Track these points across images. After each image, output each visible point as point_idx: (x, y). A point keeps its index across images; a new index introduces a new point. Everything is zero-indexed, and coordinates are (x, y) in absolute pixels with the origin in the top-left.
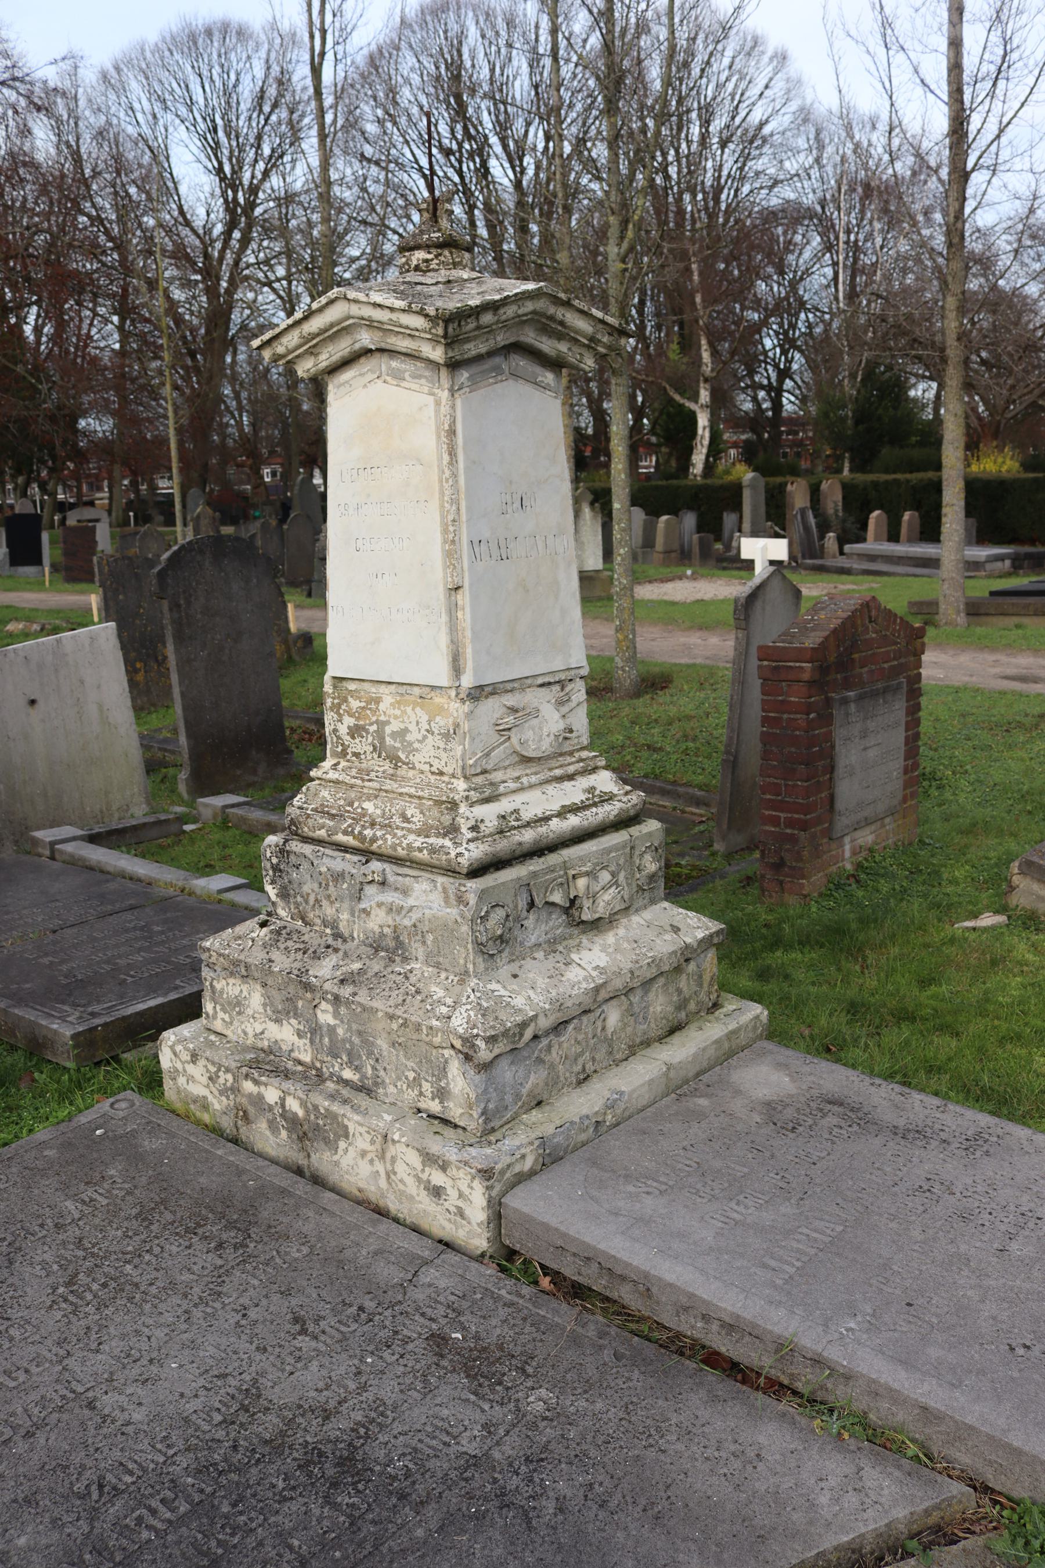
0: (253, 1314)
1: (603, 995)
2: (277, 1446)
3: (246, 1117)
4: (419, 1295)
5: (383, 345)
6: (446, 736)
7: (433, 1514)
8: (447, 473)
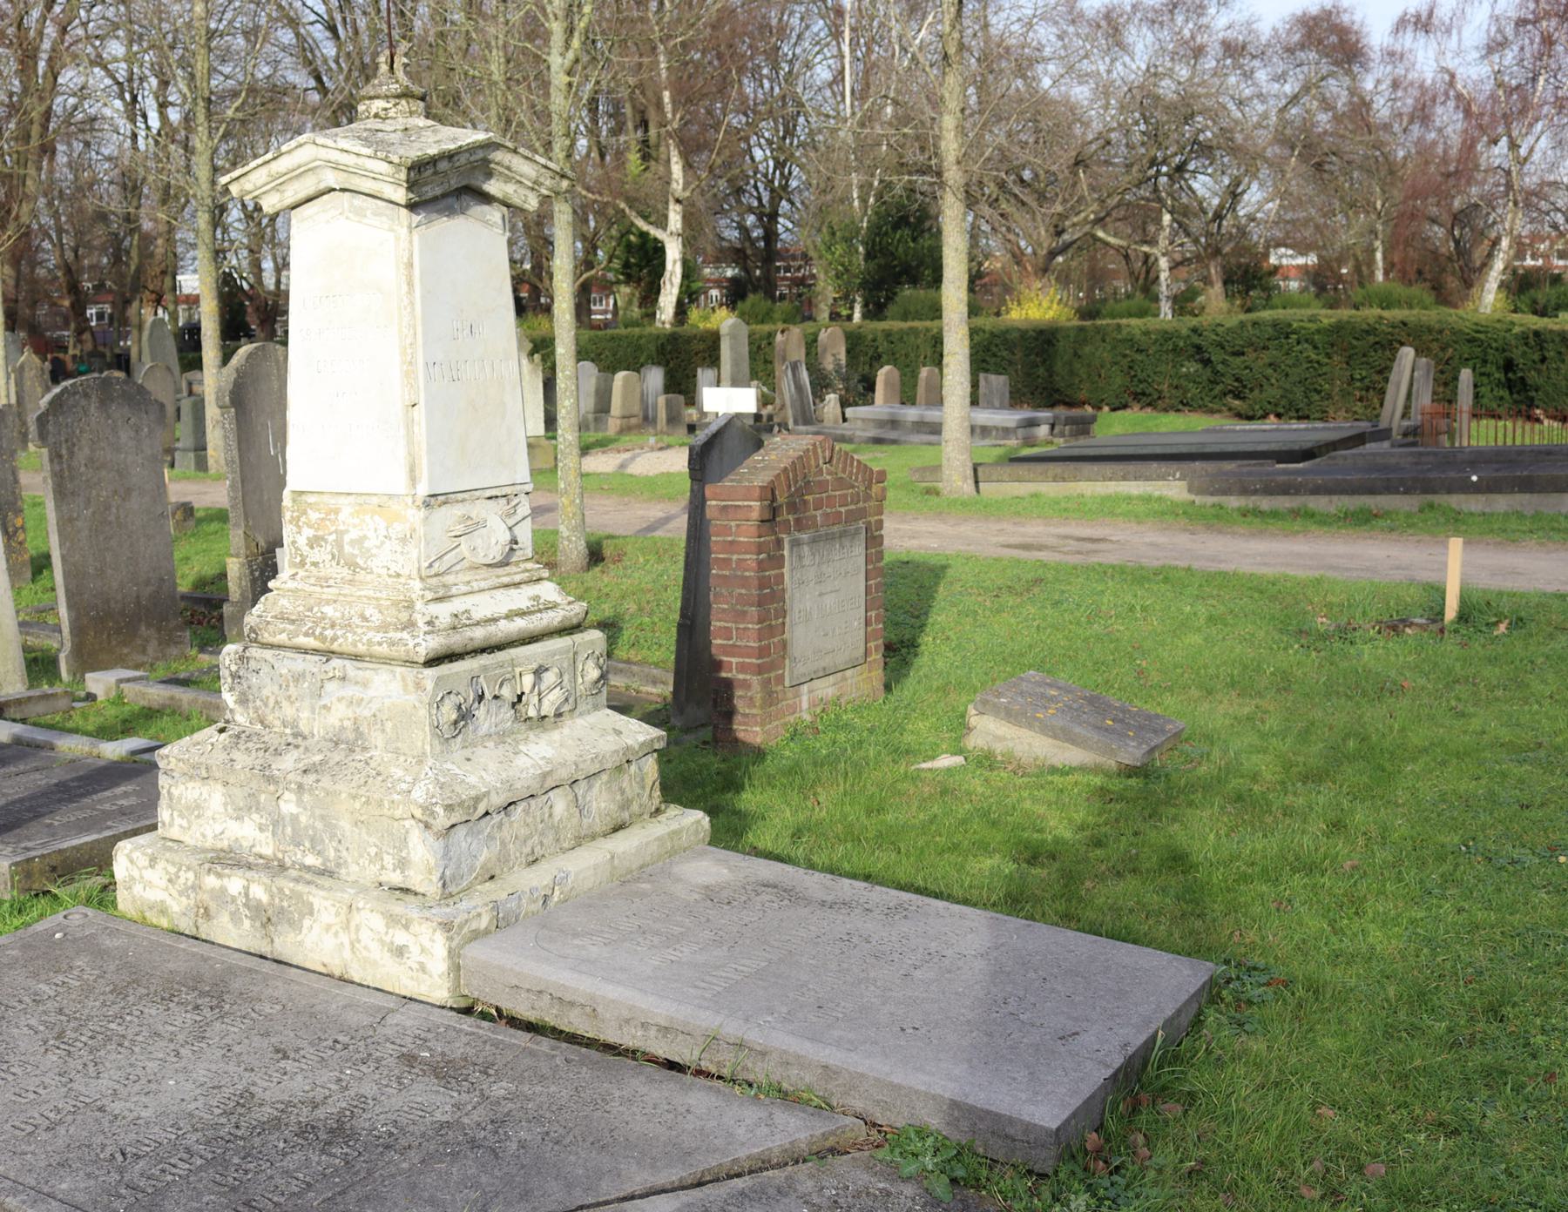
0: (237, 1049)
1: (550, 783)
2: (276, 1124)
3: (207, 914)
4: (389, 1032)
5: (347, 186)
6: (404, 540)
7: (415, 1157)
8: (406, 302)
